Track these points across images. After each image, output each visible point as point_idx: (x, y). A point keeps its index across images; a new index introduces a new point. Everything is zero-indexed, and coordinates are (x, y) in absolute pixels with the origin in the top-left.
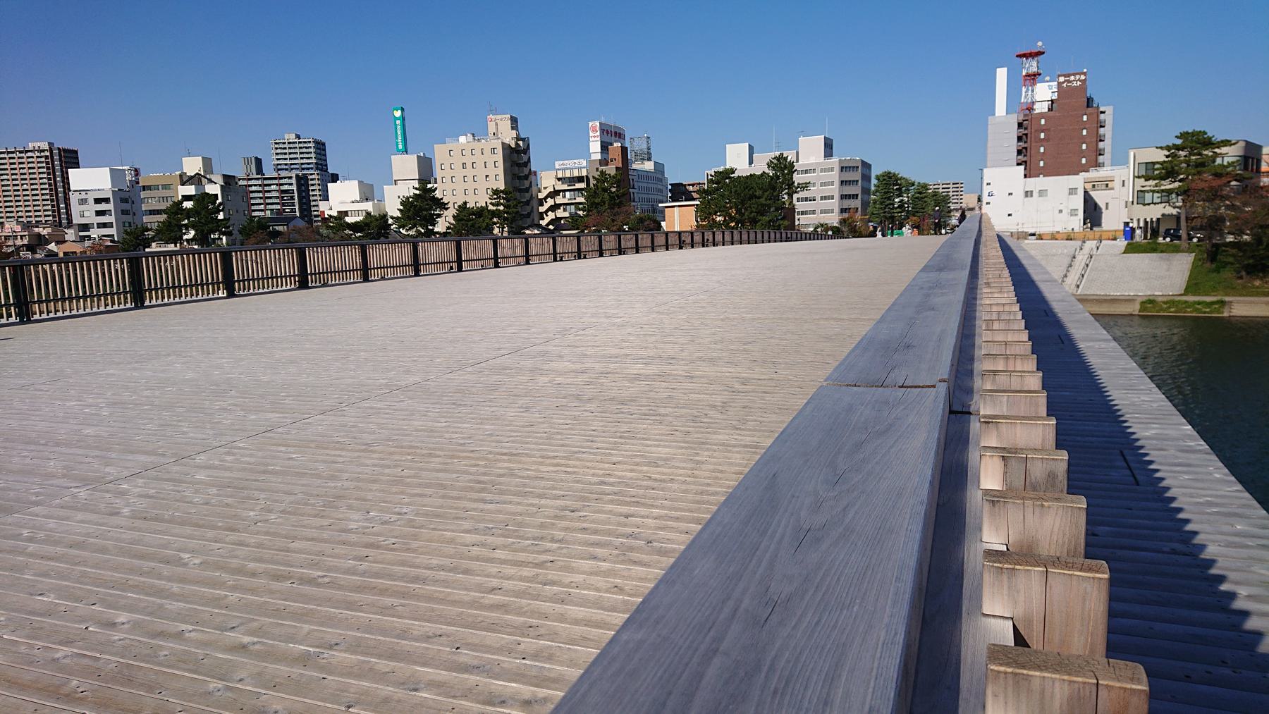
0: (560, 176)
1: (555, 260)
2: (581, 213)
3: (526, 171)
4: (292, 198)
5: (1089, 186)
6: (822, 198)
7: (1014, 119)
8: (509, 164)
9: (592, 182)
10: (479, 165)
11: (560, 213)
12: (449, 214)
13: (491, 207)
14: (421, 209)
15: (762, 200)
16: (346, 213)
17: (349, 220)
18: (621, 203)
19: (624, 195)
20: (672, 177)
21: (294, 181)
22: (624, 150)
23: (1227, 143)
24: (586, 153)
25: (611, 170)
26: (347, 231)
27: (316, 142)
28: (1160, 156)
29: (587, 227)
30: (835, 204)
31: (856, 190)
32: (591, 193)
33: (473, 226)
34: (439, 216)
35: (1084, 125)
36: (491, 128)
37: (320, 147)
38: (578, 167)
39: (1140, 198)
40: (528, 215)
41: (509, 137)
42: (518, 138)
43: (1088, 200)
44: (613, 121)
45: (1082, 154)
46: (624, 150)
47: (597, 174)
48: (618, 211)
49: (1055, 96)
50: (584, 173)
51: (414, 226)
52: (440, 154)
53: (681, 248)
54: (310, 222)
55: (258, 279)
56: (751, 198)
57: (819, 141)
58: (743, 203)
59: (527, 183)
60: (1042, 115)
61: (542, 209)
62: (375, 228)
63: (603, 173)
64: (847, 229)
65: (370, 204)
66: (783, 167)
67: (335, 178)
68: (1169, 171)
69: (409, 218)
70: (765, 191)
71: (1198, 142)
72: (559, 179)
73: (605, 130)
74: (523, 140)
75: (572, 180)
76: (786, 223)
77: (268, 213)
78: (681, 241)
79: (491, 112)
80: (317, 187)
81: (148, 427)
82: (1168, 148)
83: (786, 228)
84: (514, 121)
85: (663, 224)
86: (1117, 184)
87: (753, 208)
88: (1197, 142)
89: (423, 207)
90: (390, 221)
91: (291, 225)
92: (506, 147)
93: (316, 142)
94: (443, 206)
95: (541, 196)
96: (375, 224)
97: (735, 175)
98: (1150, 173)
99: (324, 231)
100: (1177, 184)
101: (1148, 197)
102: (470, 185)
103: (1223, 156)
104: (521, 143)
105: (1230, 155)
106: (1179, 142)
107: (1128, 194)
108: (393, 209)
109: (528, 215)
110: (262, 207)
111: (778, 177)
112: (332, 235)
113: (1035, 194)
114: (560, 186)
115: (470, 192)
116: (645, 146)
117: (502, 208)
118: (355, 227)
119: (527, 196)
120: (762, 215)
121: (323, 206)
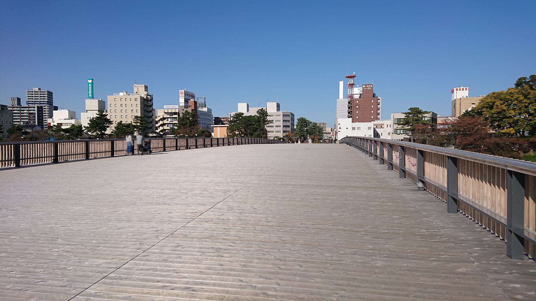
0: (166, 111)
1: (177, 149)
2: (176, 128)
3: (151, 109)
4: (34, 117)
5: (375, 126)
7: (347, 100)
8: (143, 106)
9: (181, 115)
10: (129, 105)
11: (165, 127)
13: (133, 124)
14: (99, 124)
15: (255, 126)
16: (61, 124)
17: (63, 127)
20: (215, 115)
21: (36, 109)
22: (195, 103)
24: (178, 103)
25: (190, 110)
26: (62, 133)
27: (48, 92)
28: (403, 116)
29: (179, 134)
30: (281, 129)
31: (289, 124)
32: (180, 120)
33: (124, 131)
34: (108, 127)
36: (135, 90)
37: (50, 94)
38: (175, 108)
39: (395, 132)
40: (151, 128)
41: (144, 94)
42: (148, 95)
43: (375, 131)
44: (190, 91)
46: (195, 103)
47: (184, 112)
48: (193, 128)
49: (361, 93)
50: (177, 111)
51: (96, 131)
52: (110, 100)
53: (229, 145)
54: (42, 128)
55: (45, 157)
56: (250, 125)
58: (247, 126)
59: (151, 114)
60: (357, 99)
61: (157, 125)
62: (75, 133)
63: (186, 111)
64: (287, 139)
66: (263, 113)
67: (56, 108)
68: (407, 123)
69: (93, 127)
71: (416, 112)
72: (166, 113)
73: (186, 94)
74: (150, 96)
76: (264, 135)
77: (22, 123)
78: (220, 142)
79: (135, 83)
81: (12, 274)
82: (406, 113)
83: (264, 138)
84: (146, 88)
85: (212, 134)
86: (385, 126)
87: (250, 129)
88: (416, 112)
89: (100, 122)
90: (84, 129)
91: (34, 129)
92: (142, 98)
93: (48, 92)
94: (110, 122)
95: (157, 120)
97: (244, 115)
99: (50, 132)
100: (409, 127)
101: (399, 131)
102: (124, 114)
103: (425, 117)
104: (149, 97)
105: (427, 117)
106: (410, 111)
107: (391, 130)
108: (85, 122)
109: (151, 128)
110: (19, 120)
111: (261, 117)
112: (54, 134)
113: (356, 129)
114: (166, 116)
116: (203, 101)
117: (139, 124)
118: (66, 131)
119: (151, 119)
120: (255, 132)
121: (49, 121)
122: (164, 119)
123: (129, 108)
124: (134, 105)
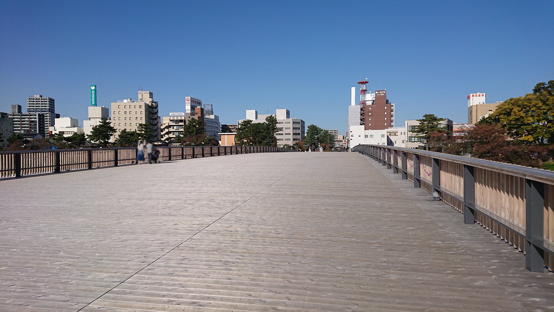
0: (172, 119)
1: (183, 158)
2: (182, 136)
3: (156, 116)
4: (36, 125)
6: (286, 134)
7: (359, 107)
8: (148, 113)
9: (187, 123)
11: (171, 135)
12: (117, 135)
13: (138, 132)
14: (103, 132)
15: (264, 134)
16: (63, 133)
17: (65, 136)
18: (201, 132)
19: (202, 129)
20: (222, 122)
21: (37, 117)
22: (202, 110)
23: (441, 119)
25: (196, 117)
26: (64, 141)
28: (418, 123)
30: (291, 137)
32: (187, 128)
33: (128, 140)
34: (112, 135)
35: (385, 111)
36: (140, 97)
37: (52, 101)
38: (181, 115)
39: (410, 139)
40: (156, 136)
41: (148, 101)
42: (153, 102)
44: (196, 97)
45: (385, 121)
46: (202, 110)
48: (199, 137)
50: (183, 118)
51: (99, 139)
52: (114, 107)
56: (259, 132)
57: (285, 111)
58: (255, 134)
59: (156, 122)
60: (369, 106)
61: (162, 133)
62: (78, 141)
63: (193, 119)
64: (298, 147)
65: (76, 128)
66: (272, 121)
67: (58, 116)
69: (96, 136)
70: (265, 130)
72: (171, 121)
73: (193, 101)
74: (155, 103)
75: (178, 121)
76: (274, 144)
77: (22, 131)
78: (227, 151)
79: (140, 90)
80: (48, 122)
82: (420, 121)
83: (273, 146)
84: (151, 95)
85: (220, 142)
87: (259, 137)
88: (431, 119)
89: (103, 130)
90: (86, 137)
91: (35, 138)
92: (146, 105)
94: (114, 131)
95: (162, 127)
96: (78, 138)
97: (252, 123)
98: (413, 130)
99: (51, 141)
100: (424, 135)
101: (413, 139)
103: (440, 124)
104: (154, 104)
105: (443, 124)
106: (424, 118)
107: (405, 138)
108: (88, 130)
109: (156, 136)
111: (270, 125)
112: (56, 143)
114: (171, 123)
115: (128, 125)
116: (210, 108)
117: (143, 132)
118: (68, 139)
120: (263, 140)
121: (51, 129)
122: (169, 126)
123: (133, 116)
124: (139, 113)
